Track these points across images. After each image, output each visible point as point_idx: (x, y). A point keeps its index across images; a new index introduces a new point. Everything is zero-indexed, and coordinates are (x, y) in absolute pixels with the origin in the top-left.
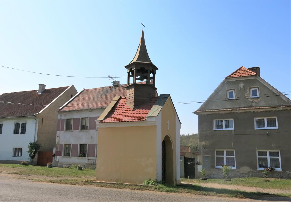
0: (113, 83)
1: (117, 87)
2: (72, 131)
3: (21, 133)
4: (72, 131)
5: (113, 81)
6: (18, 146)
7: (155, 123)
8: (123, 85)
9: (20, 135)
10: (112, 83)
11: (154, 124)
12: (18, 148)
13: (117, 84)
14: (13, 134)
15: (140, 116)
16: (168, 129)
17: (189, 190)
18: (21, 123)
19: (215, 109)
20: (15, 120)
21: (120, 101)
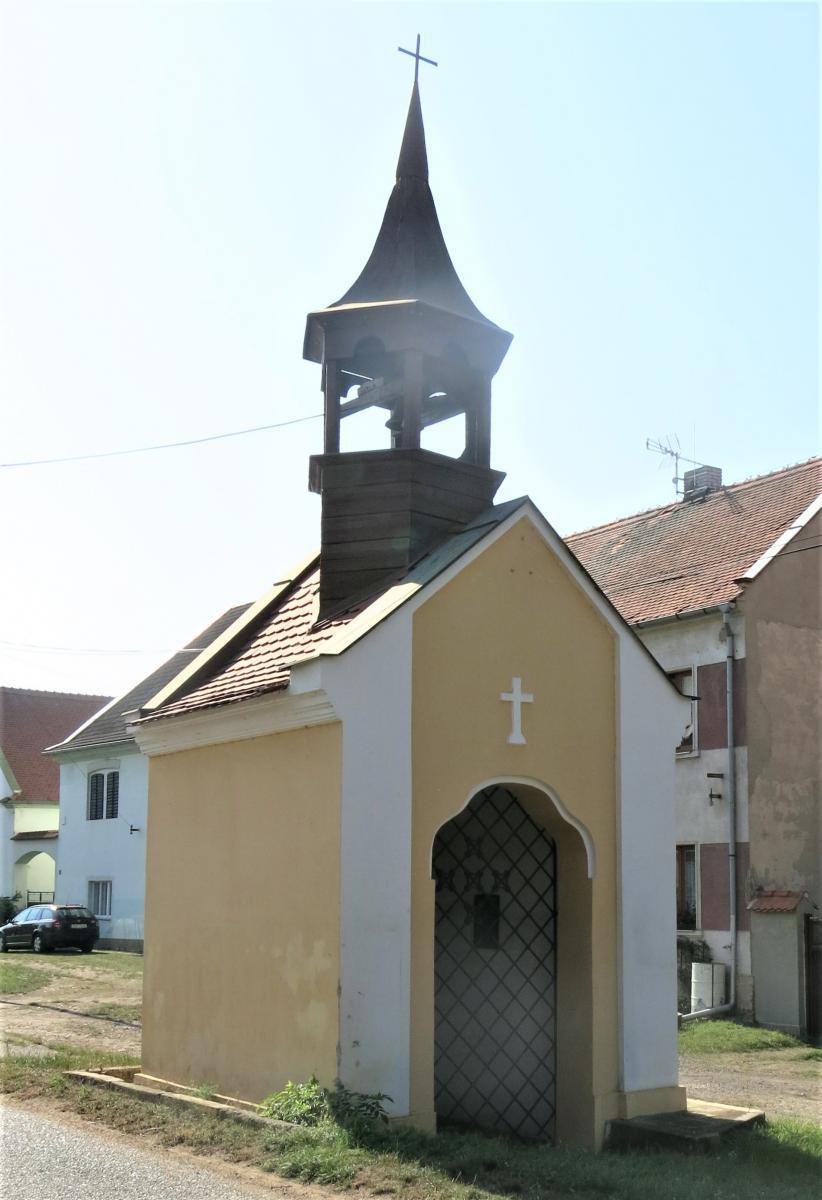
0: (681, 486)
1: (703, 501)
2: (695, 754)
3: (108, 817)
4: (695, 754)
5: (686, 467)
6: (99, 876)
7: (329, 705)
8: (733, 487)
9: (104, 823)
10: (675, 481)
11: (324, 716)
12: (103, 879)
13: (706, 487)
14: (87, 819)
15: (235, 676)
16: (517, 737)
17: (411, 1169)
18: (106, 773)
19: (603, 527)
20: (88, 762)
21: (303, 585)
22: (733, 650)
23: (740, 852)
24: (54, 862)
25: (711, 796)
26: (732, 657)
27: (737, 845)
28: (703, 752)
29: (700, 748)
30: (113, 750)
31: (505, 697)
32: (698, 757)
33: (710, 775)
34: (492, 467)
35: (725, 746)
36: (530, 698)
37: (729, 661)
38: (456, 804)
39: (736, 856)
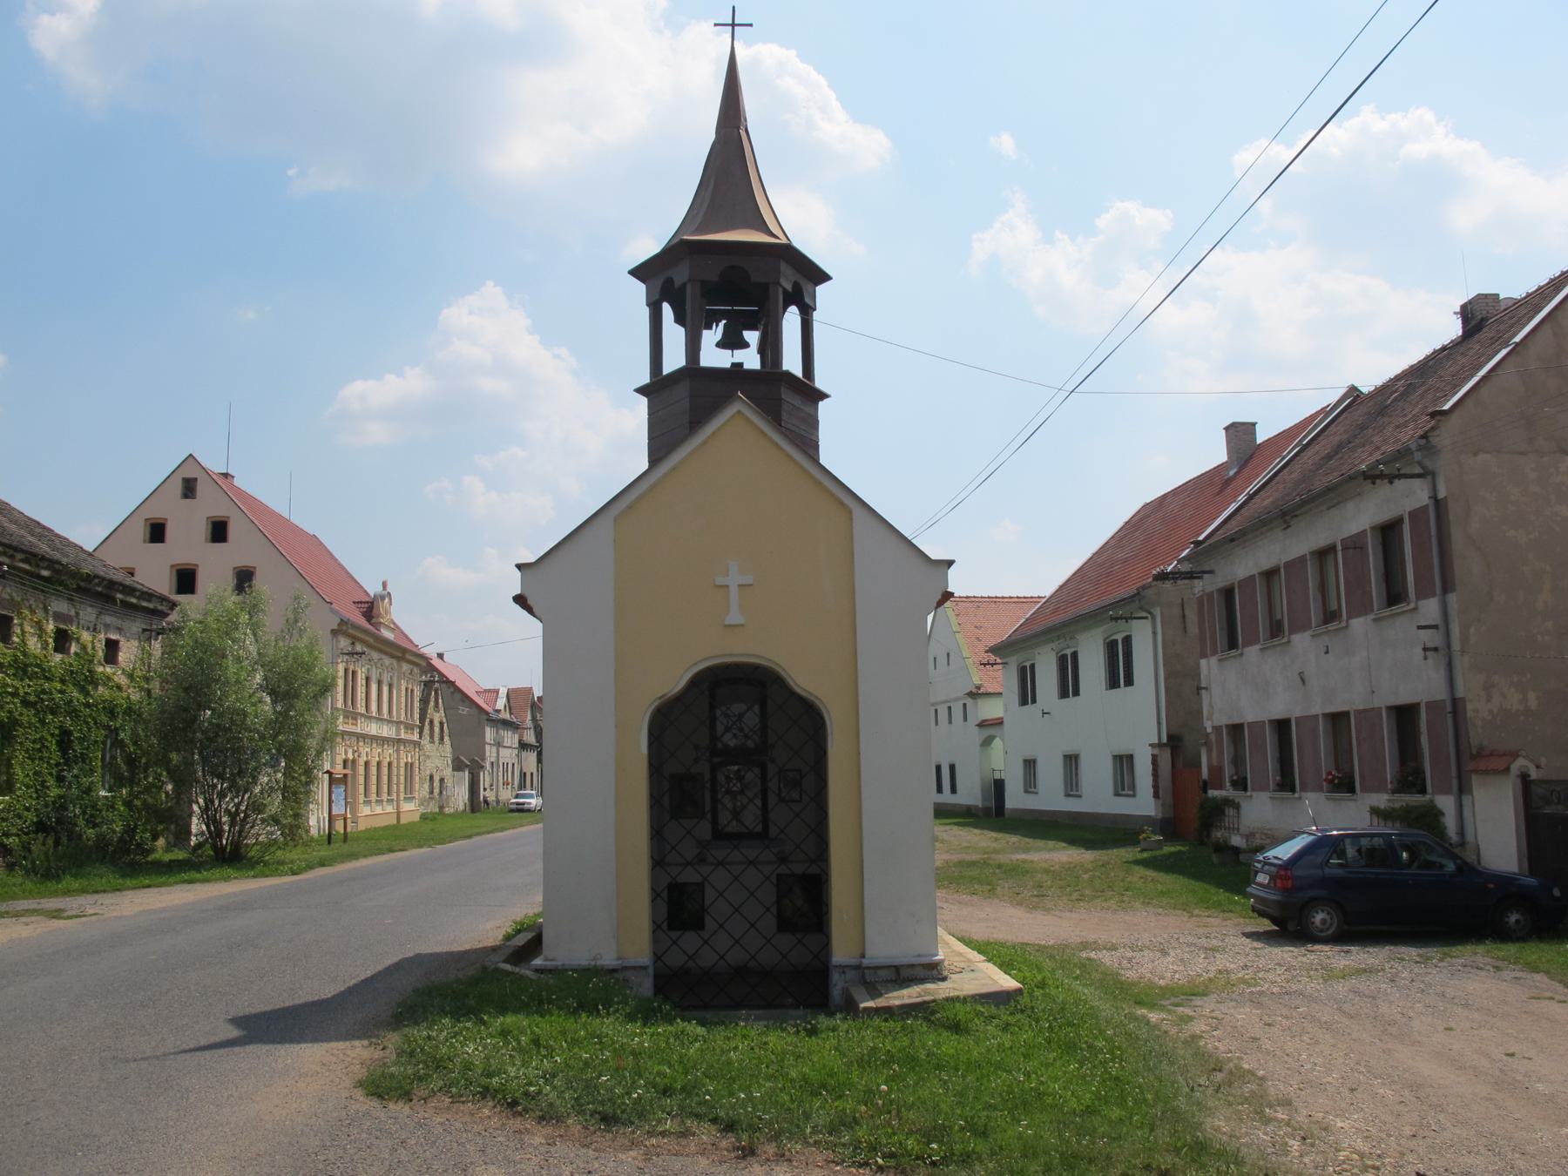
2: (1412, 605)
4: (1412, 605)
22: (1434, 489)
23: (1457, 706)
24: (646, 466)
25: (1425, 649)
26: (1434, 498)
27: (1455, 701)
28: (1421, 603)
29: (1418, 599)
30: (1070, 613)
31: (720, 580)
32: (1415, 609)
33: (1419, 627)
34: (683, 363)
35: (1434, 595)
36: (748, 579)
37: (1431, 503)
38: (674, 680)
39: (1455, 713)
